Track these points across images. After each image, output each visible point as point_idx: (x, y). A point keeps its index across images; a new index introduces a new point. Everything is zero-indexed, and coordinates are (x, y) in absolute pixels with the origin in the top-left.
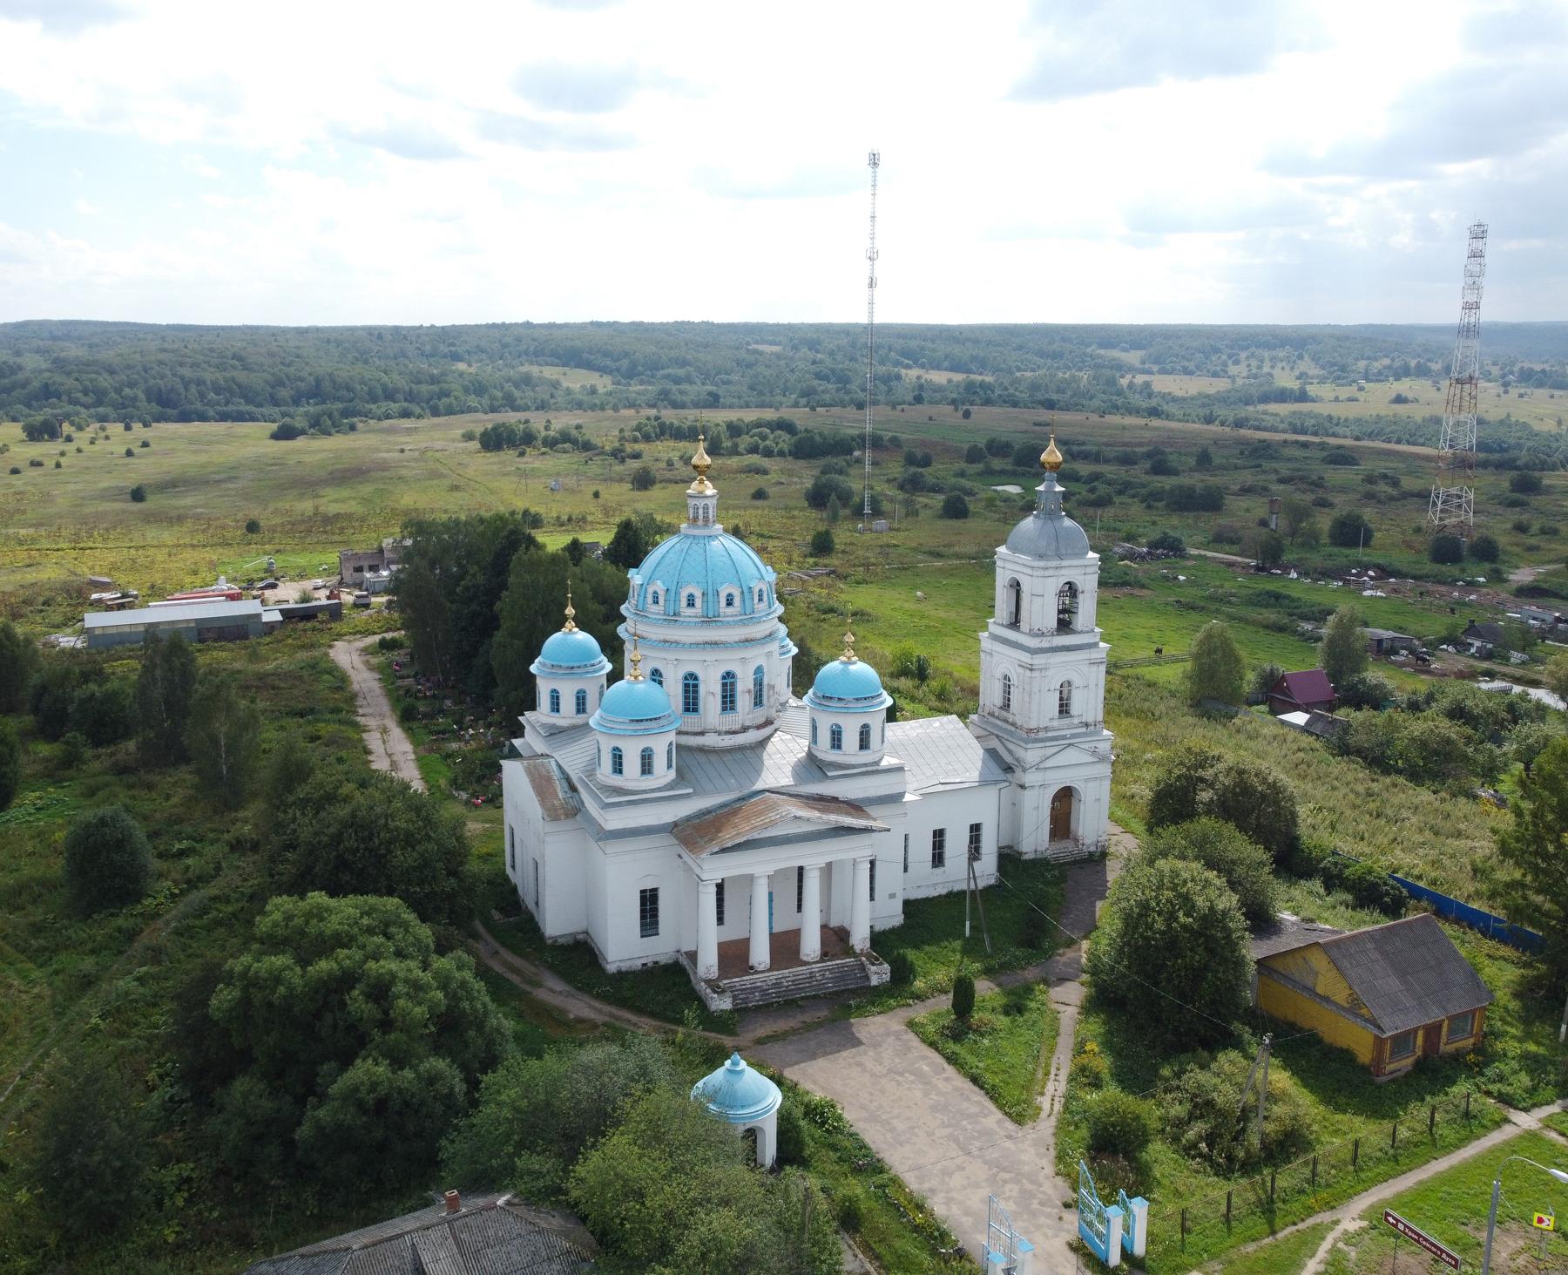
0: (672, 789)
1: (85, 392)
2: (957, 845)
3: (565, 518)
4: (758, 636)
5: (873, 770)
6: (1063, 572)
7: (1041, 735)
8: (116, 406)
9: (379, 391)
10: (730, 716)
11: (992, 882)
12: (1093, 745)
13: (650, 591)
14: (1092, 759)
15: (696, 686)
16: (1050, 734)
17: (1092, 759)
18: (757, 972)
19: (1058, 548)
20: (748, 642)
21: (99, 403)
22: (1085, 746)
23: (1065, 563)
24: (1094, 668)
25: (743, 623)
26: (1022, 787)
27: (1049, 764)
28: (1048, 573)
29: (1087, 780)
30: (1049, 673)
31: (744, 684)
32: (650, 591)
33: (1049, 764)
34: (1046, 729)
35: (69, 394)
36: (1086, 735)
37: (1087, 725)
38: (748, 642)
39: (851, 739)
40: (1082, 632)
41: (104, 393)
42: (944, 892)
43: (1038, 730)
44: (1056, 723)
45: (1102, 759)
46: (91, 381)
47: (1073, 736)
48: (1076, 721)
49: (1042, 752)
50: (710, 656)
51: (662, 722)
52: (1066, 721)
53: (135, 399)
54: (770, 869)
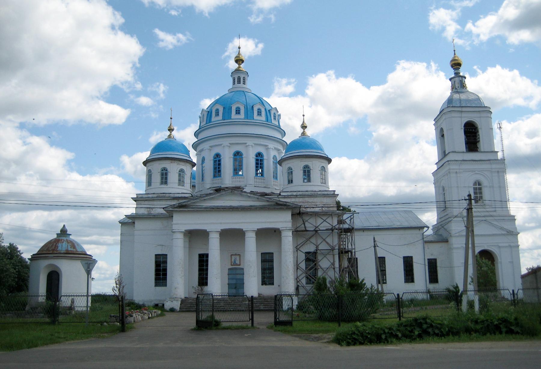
28: (453, 114)
54: (220, 228)
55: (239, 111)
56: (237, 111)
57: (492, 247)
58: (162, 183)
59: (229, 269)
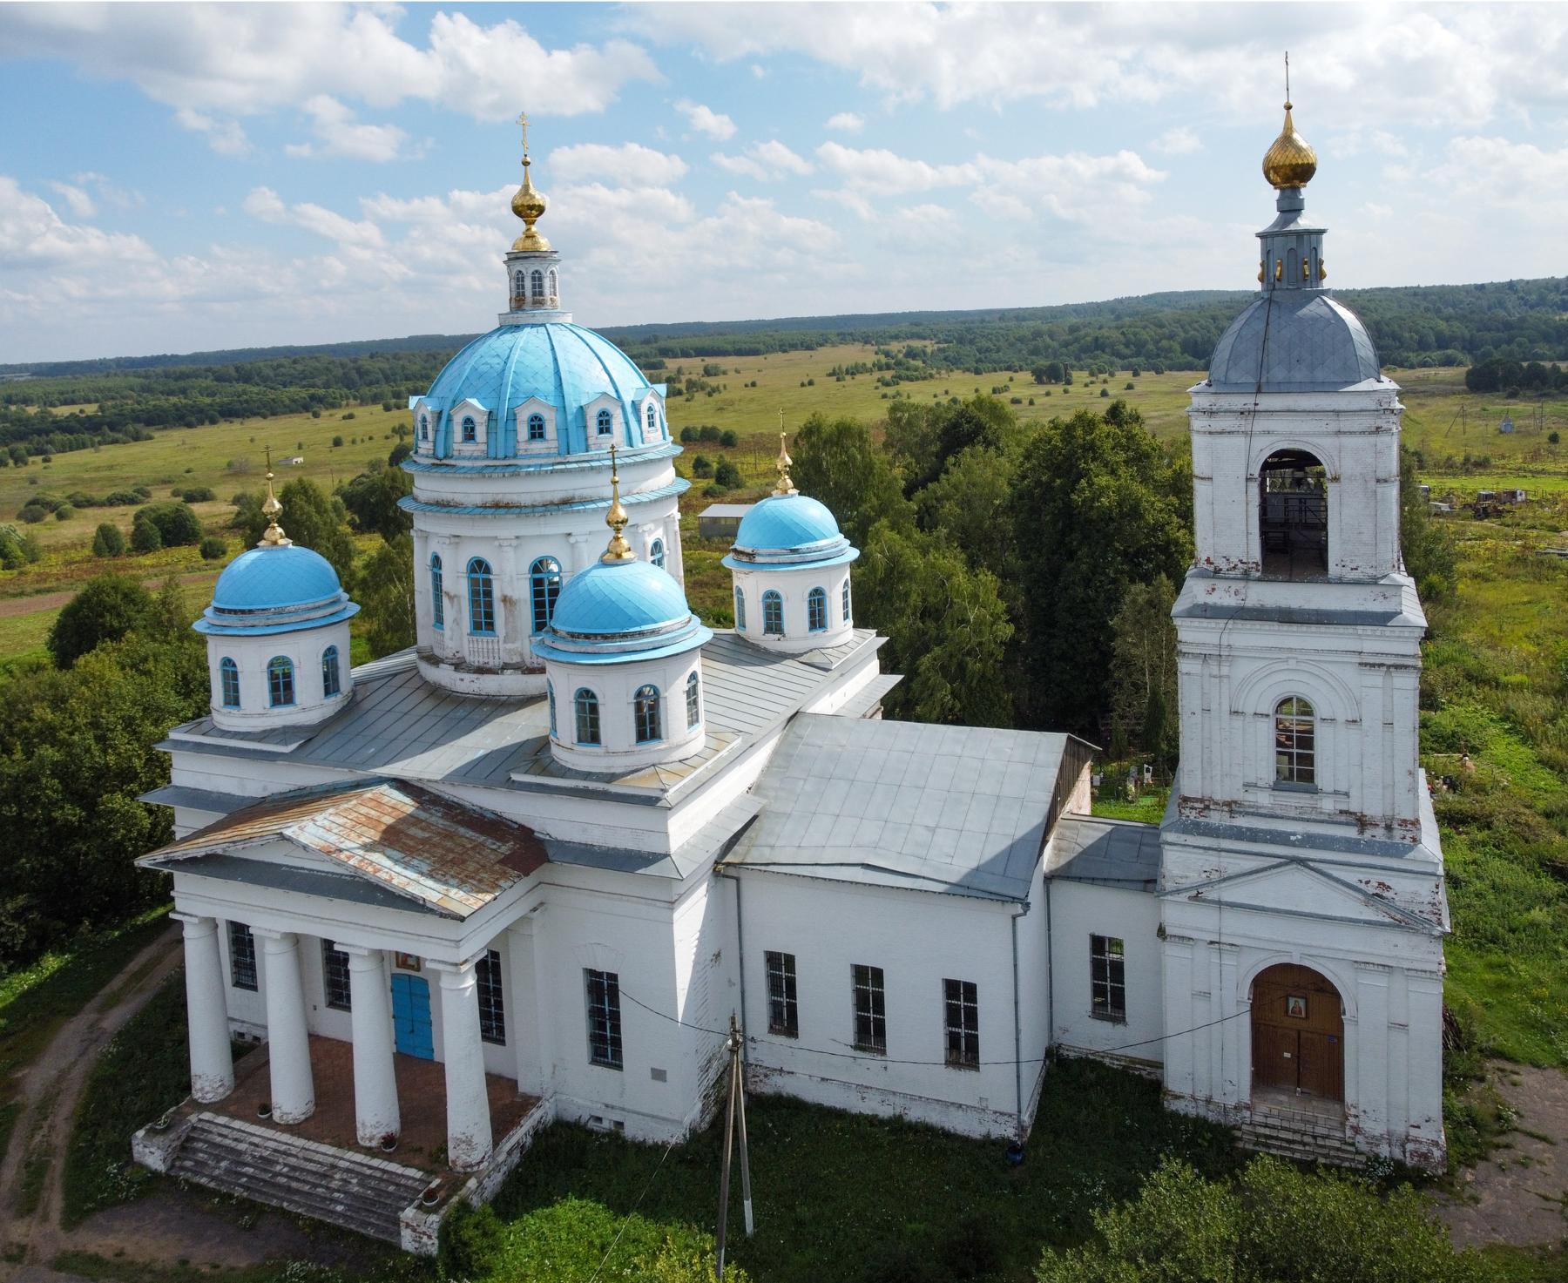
0: (260, 741)
1: (1127, 345)
2: (916, 1019)
3: (1459, 459)
4: (525, 500)
5: (598, 790)
6: (1261, 424)
7: (1216, 818)
8: (1149, 356)
9: (1432, 339)
10: (484, 641)
11: (1008, 1131)
12: (1376, 877)
13: (458, 419)
14: (1369, 914)
15: (488, 583)
16: (1242, 822)
17: (1369, 914)
18: (270, 1123)
19: (1261, 366)
20: (499, 508)
21: (1138, 354)
22: (1352, 876)
23: (1266, 402)
24: (1376, 678)
25: (482, 473)
26: (1161, 932)
27: (1231, 893)
29: (1361, 965)
30: (1243, 669)
31: (512, 582)
32: (458, 419)
33: (1231, 893)
34: (1232, 807)
35: (1112, 345)
36: (1351, 846)
37: (1362, 822)
38: (499, 508)
39: (617, 720)
40: (1340, 582)
41: (1144, 344)
42: (885, 1112)
43: (1206, 804)
44: (1264, 799)
45: (1405, 922)
46: (1135, 334)
47: (1310, 841)
48: (1328, 805)
49: (1212, 860)
50: (506, 529)
51: (250, 620)
52: (1294, 801)
53: (1170, 350)
55: (541, 427)
56: (533, 427)
57: (1331, 965)
58: (276, 702)
59: (394, 976)
